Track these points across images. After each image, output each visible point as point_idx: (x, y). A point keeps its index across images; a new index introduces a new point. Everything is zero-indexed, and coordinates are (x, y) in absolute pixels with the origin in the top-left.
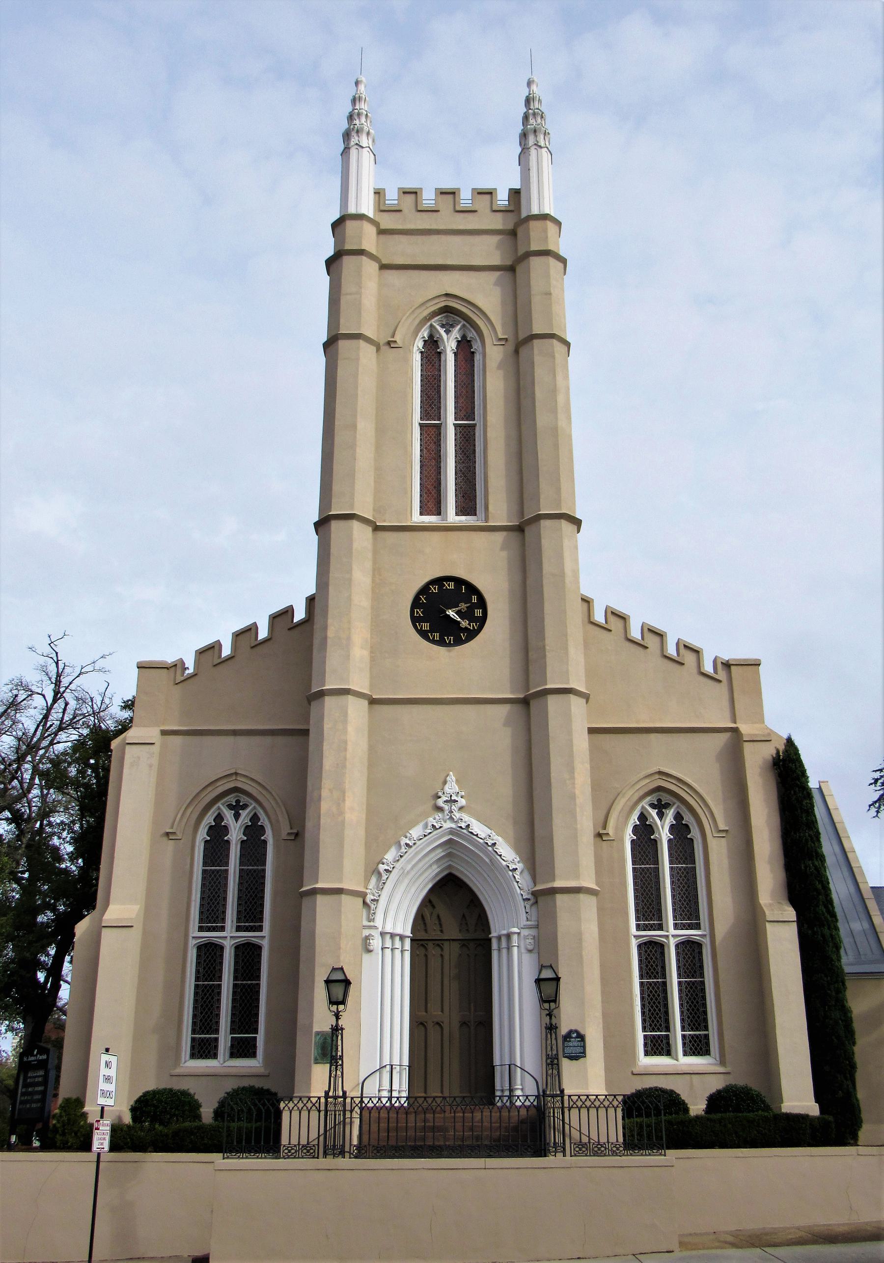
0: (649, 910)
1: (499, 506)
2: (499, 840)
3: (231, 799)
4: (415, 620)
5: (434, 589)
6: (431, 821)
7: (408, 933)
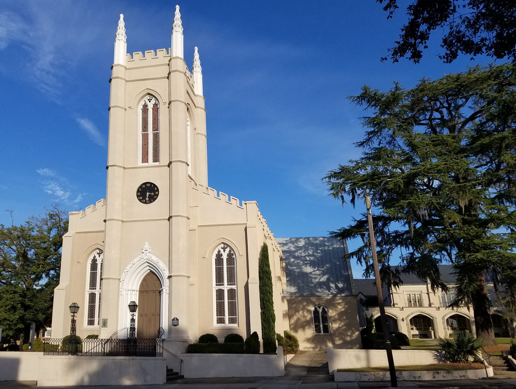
0: (219, 280)
1: (164, 159)
2: (160, 261)
3: (222, 245)
4: (138, 196)
5: (144, 186)
6: (140, 256)
7: (138, 289)
